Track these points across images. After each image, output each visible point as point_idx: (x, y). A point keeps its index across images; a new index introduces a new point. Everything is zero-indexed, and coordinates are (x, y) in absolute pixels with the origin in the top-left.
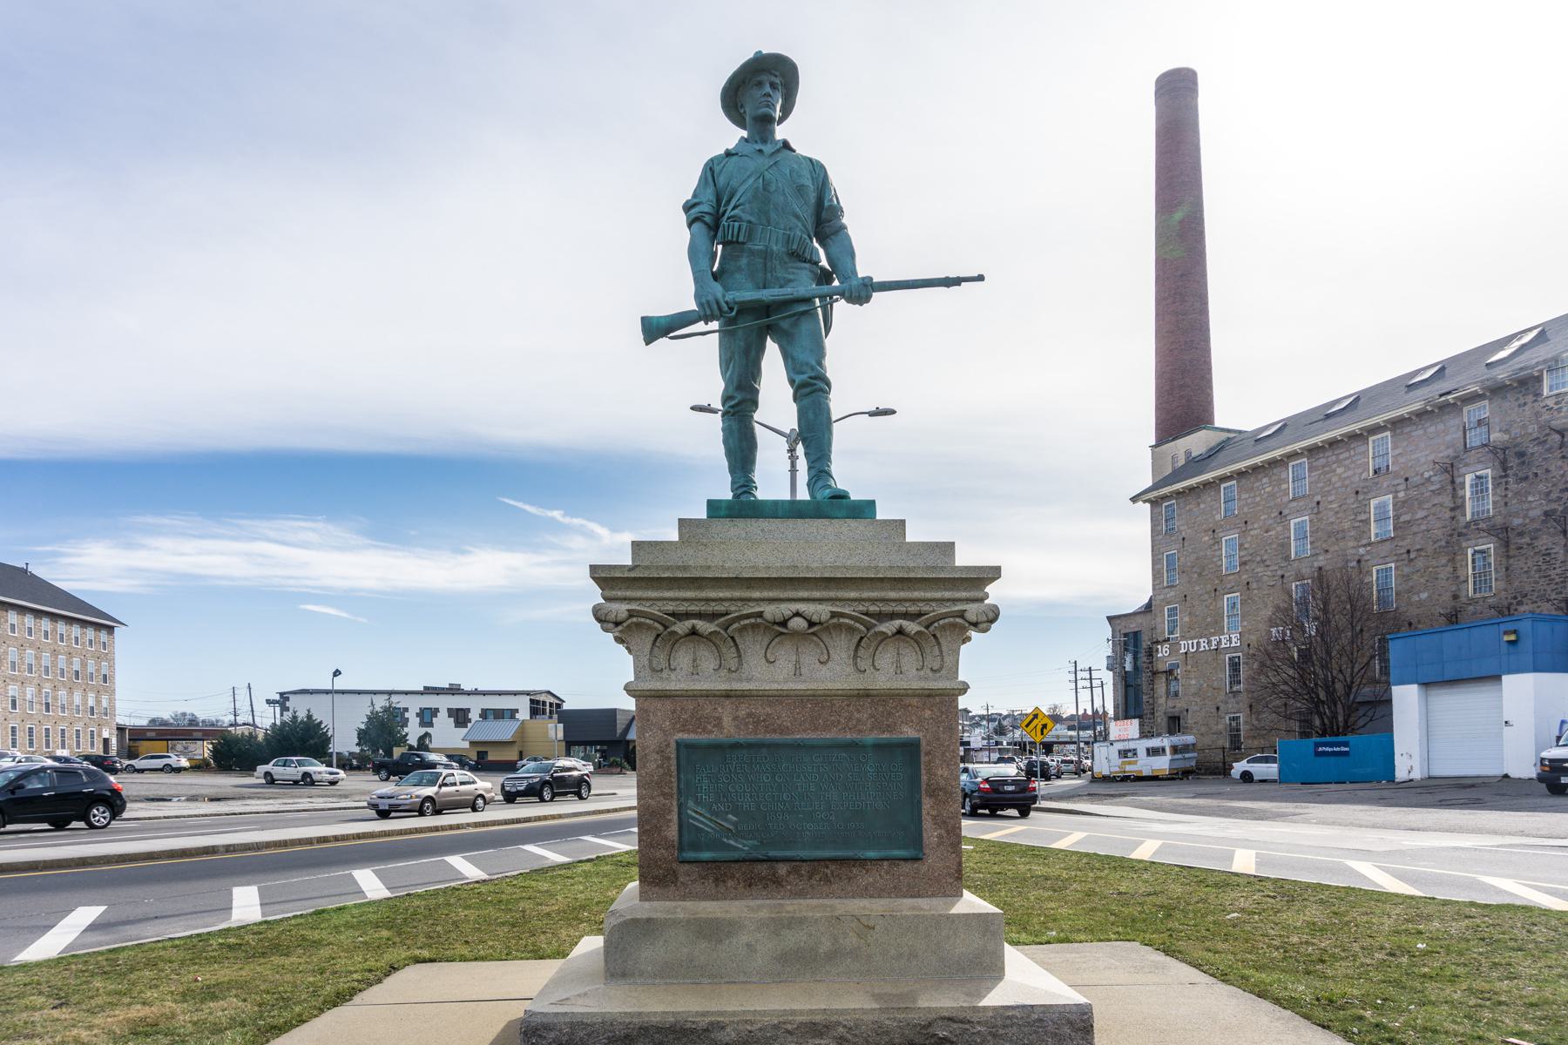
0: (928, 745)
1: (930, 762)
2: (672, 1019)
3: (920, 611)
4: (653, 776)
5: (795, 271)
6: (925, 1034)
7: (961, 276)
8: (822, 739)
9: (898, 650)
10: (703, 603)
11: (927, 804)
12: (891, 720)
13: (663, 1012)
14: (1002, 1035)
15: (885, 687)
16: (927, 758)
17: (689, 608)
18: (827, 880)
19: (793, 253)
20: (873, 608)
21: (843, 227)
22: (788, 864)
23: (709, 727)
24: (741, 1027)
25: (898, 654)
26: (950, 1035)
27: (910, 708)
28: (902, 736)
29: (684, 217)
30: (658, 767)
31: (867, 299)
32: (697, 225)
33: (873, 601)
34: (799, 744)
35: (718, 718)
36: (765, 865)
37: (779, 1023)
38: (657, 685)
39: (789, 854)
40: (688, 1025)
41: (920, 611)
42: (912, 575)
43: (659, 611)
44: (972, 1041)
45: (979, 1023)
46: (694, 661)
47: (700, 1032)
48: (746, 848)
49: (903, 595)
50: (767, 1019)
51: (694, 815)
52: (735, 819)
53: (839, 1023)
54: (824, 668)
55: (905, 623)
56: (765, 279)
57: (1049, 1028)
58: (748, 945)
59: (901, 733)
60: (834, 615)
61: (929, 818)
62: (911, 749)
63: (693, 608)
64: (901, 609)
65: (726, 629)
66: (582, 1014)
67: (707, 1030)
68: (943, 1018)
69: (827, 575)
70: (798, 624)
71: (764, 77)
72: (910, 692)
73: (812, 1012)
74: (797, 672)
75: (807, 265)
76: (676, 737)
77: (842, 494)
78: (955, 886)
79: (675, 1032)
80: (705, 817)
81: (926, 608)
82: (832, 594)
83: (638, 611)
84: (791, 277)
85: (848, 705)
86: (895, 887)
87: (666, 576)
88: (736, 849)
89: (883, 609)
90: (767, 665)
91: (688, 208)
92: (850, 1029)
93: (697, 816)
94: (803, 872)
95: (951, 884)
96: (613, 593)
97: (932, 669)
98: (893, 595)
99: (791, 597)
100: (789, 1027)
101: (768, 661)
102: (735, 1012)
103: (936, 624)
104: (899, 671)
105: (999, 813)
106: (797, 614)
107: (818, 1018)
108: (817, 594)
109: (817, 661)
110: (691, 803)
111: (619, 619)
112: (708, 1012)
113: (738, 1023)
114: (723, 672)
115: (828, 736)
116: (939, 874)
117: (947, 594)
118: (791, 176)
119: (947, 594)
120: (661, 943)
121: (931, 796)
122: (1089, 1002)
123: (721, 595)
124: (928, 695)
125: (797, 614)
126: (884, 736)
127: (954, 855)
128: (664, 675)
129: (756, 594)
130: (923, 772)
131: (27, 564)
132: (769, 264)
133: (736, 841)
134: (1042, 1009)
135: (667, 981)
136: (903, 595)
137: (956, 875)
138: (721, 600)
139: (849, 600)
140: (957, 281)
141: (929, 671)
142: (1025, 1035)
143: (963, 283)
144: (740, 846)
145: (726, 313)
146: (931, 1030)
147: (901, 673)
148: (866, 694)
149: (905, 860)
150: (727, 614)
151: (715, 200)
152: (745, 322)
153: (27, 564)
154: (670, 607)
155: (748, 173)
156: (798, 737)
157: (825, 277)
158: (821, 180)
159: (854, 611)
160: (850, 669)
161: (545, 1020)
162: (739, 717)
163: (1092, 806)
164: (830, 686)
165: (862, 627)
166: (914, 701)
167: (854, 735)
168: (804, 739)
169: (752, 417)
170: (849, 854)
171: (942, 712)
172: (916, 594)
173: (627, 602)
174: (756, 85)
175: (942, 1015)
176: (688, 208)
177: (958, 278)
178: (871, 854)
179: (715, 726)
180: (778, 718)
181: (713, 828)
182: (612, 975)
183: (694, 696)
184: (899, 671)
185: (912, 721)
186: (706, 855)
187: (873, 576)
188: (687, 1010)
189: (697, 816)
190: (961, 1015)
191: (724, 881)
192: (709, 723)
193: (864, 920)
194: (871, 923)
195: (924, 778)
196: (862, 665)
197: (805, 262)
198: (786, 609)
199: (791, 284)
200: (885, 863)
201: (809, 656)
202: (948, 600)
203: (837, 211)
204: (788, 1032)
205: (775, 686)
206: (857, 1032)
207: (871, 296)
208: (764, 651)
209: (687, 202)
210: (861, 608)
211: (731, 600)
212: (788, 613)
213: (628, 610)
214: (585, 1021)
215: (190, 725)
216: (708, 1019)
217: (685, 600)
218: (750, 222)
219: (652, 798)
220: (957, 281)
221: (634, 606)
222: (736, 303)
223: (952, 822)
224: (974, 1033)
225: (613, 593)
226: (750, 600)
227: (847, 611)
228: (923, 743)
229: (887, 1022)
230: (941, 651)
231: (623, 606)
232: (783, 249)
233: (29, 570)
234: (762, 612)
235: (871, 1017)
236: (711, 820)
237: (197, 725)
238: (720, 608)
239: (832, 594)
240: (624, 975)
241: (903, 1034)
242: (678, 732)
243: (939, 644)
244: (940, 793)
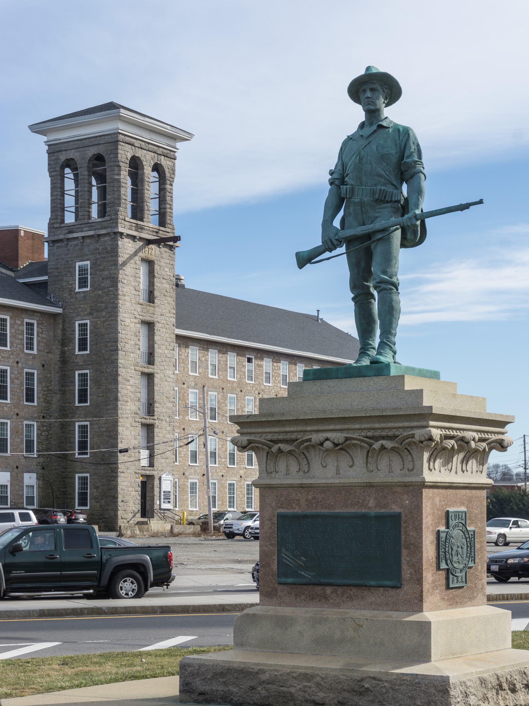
0: (405, 517)
1: (406, 527)
2: (243, 666)
3: (394, 434)
4: (267, 533)
5: (380, 210)
6: (359, 685)
7: (469, 202)
8: (349, 512)
9: (389, 458)
10: (285, 434)
11: (404, 552)
12: (386, 501)
13: (240, 662)
14: (397, 689)
15: (379, 481)
16: (405, 525)
17: (279, 437)
18: (351, 598)
19: (377, 200)
20: (370, 434)
22: (331, 587)
23: (294, 505)
24: (272, 673)
25: (390, 460)
26: (370, 687)
27: (396, 494)
28: (391, 511)
30: (269, 528)
33: (369, 429)
34: (336, 516)
35: (298, 500)
36: (320, 587)
37: (290, 672)
38: (268, 481)
39: (331, 581)
40: (250, 670)
41: (394, 434)
42: (384, 414)
43: (265, 439)
44: (381, 691)
45: (386, 681)
46: (287, 466)
47: (255, 674)
48: (310, 577)
49: (383, 425)
50: (285, 670)
51: (285, 556)
52: (304, 559)
53: (318, 675)
54: (352, 470)
55: (384, 442)
56: (363, 218)
57: (422, 688)
58: (300, 632)
59: (391, 509)
60: (347, 439)
61: (405, 562)
62: (396, 518)
63: (281, 437)
64: (384, 433)
65: (298, 448)
66: (204, 659)
67: (257, 673)
68: (370, 677)
69: (341, 416)
70: (328, 444)
71: (365, 87)
72: (393, 484)
73: (307, 668)
74: (338, 473)
75: (389, 205)
76: (278, 511)
77: (375, 360)
78: (419, 605)
79: (243, 673)
80: (290, 558)
81: (397, 433)
82: (346, 426)
83: (253, 440)
84: (377, 215)
85: (363, 492)
86: (386, 604)
87: (263, 420)
88: (305, 577)
89: (374, 434)
90: (322, 468)
92: (323, 678)
93: (286, 557)
94: (339, 592)
95: (416, 604)
96: (245, 431)
97: (408, 469)
98: (377, 425)
99: (326, 429)
100: (294, 675)
101: (323, 467)
102: (271, 664)
103: (404, 442)
104: (391, 471)
106: (327, 439)
107: (309, 671)
108: (338, 427)
109: (347, 466)
110: (283, 550)
111: (243, 445)
112: (259, 663)
113: (271, 671)
114: (301, 473)
115: (353, 511)
116: (410, 598)
117: (406, 424)
118: (377, 150)
119: (406, 424)
120: (259, 628)
121: (406, 548)
123: (292, 429)
124: (406, 485)
125: (327, 439)
126: (382, 511)
127: (418, 586)
128: (273, 475)
129: (309, 428)
130: (402, 533)
131: (318, 311)
132: (363, 209)
133: (305, 572)
134: (422, 677)
135: (262, 650)
136: (383, 425)
137: (420, 598)
138: (291, 432)
139: (355, 429)
140: (466, 207)
141: (407, 471)
142: (410, 690)
143: (471, 207)
144: (307, 575)
146: (362, 683)
147: (392, 472)
148: (370, 486)
149: (392, 587)
150: (297, 440)
151: (342, 170)
152: (355, 247)
153: (318, 311)
154: (269, 437)
155: (353, 153)
156: (338, 511)
158: (404, 144)
159: (360, 436)
160: (365, 470)
161: (189, 662)
162: (308, 499)
163: (157, 542)
164: (351, 480)
165: (366, 445)
166: (399, 489)
167: (367, 511)
168: (340, 512)
170: (361, 582)
171: (413, 496)
172: (390, 425)
173: (249, 435)
174: (363, 92)
175: (370, 675)
178: (372, 583)
179: (297, 504)
180: (328, 500)
181: (293, 564)
182: (237, 645)
183: (286, 487)
184: (391, 471)
185: (397, 502)
186: (290, 580)
187: (364, 415)
188: (250, 661)
189: (286, 557)
190: (379, 676)
191: (300, 596)
192: (294, 503)
193: (357, 621)
194: (361, 624)
195: (403, 537)
196: (371, 467)
197: (387, 202)
198: (321, 436)
200: (381, 589)
201: (344, 462)
202: (408, 427)
204: (293, 677)
205: (324, 481)
206: (326, 681)
208: (320, 460)
210: (363, 434)
211: (297, 431)
212: (322, 439)
213: (248, 440)
214: (206, 663)
215: (503, 479)
216: (258, 668)
217: (275, 433)
218: (352, 185)
219: (266, 546)
220: (466, 207)
221: (252, 438)
223: (418, 565)
224: (382, 687)
225: (245, 431)
226: (307, 431)
227: (355, 436)
228: (403, 515)
229: (341, 677)
230: (413, 458)
231: (245, 438)
232: (371, 199)
233: (320, 317)
234: (311, 438)
235: (334, 673)
236: (293, 560)
237: (510, 479)
238: (293, 436)
239: (346, 426)
240: (242, 645)
241: (349, 684)
242: (279, 508)
243: (410, 453)
244: (412, 547)
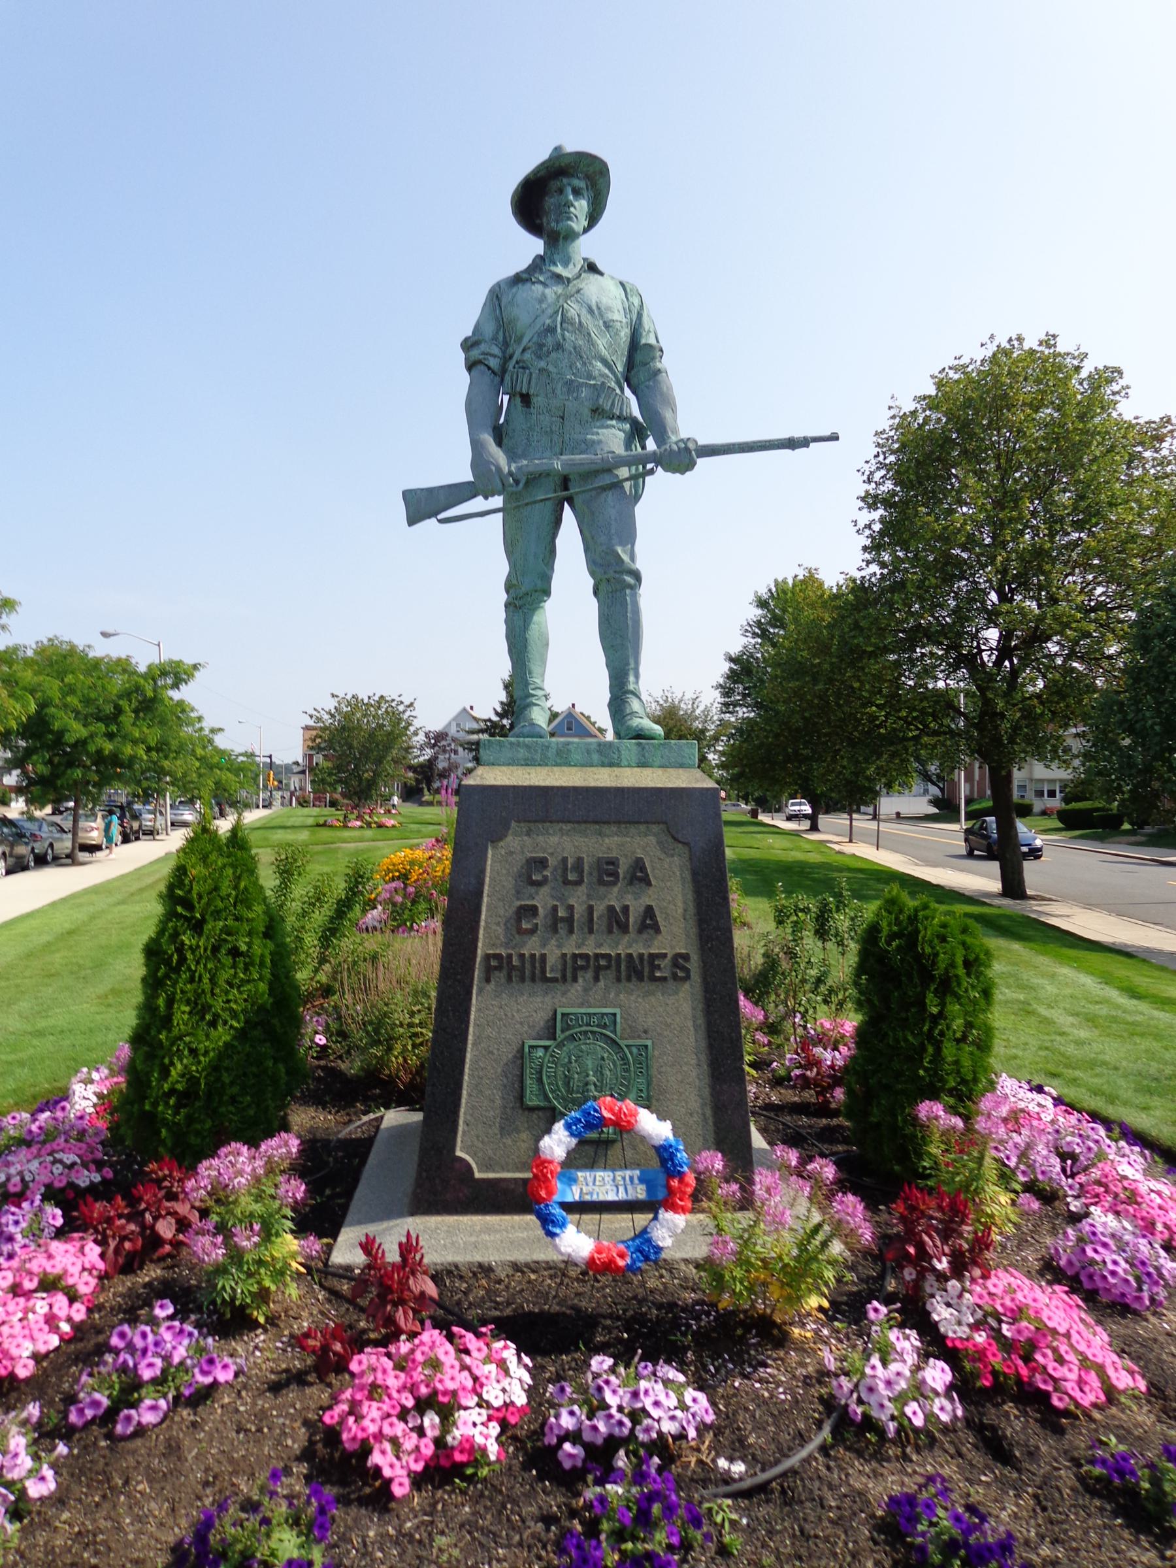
29: (461, 356)
75: (614, 422)
140: (805, 442)
176: (468, 345)
207: (695, 463)
220: (805, 442)
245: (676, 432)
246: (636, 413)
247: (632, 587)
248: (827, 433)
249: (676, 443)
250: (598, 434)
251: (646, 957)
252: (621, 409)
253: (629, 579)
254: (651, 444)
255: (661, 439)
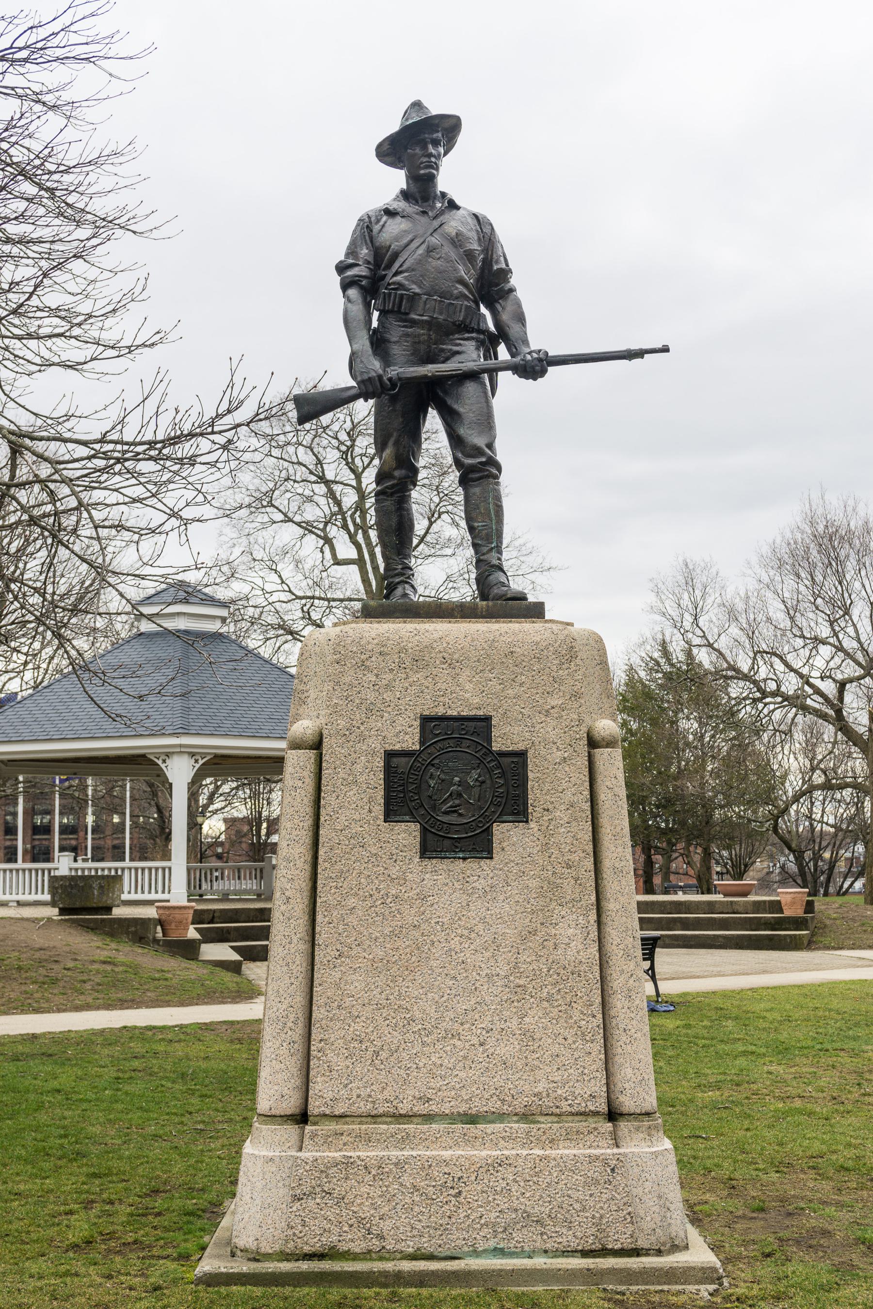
5: (462, 342)
21: (512, 290)
29: (337, 279)
31: (542, 373)
32: (353, 292)
75: (474, 335)
91: (341, 268)
105: (492, 328)
122: (689, 1226)
140: (639, 354)
145: (390, 390)
157: (490, 349)
169: (410, 496)
177: (641, 350)
199: (458, 358)
203: (505, 274)
207: (546, 371)
209: (341, 262)
220: (639, 354)
222: (400, 379)
245: (526, 342)
246: (492, 328)
247: (497, 477)
248: (659, 345)
249: (530, 353)
250: (460, 345)
251: (14, 843)
252: (479, 324)
253: (495, 471)
254: (503, 352)
255: (513, 351)
